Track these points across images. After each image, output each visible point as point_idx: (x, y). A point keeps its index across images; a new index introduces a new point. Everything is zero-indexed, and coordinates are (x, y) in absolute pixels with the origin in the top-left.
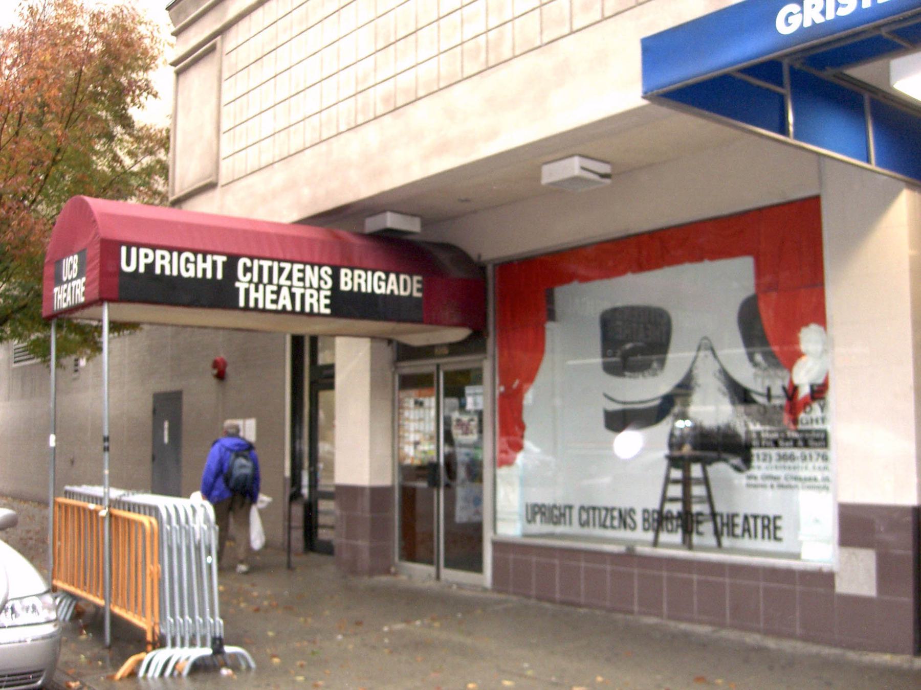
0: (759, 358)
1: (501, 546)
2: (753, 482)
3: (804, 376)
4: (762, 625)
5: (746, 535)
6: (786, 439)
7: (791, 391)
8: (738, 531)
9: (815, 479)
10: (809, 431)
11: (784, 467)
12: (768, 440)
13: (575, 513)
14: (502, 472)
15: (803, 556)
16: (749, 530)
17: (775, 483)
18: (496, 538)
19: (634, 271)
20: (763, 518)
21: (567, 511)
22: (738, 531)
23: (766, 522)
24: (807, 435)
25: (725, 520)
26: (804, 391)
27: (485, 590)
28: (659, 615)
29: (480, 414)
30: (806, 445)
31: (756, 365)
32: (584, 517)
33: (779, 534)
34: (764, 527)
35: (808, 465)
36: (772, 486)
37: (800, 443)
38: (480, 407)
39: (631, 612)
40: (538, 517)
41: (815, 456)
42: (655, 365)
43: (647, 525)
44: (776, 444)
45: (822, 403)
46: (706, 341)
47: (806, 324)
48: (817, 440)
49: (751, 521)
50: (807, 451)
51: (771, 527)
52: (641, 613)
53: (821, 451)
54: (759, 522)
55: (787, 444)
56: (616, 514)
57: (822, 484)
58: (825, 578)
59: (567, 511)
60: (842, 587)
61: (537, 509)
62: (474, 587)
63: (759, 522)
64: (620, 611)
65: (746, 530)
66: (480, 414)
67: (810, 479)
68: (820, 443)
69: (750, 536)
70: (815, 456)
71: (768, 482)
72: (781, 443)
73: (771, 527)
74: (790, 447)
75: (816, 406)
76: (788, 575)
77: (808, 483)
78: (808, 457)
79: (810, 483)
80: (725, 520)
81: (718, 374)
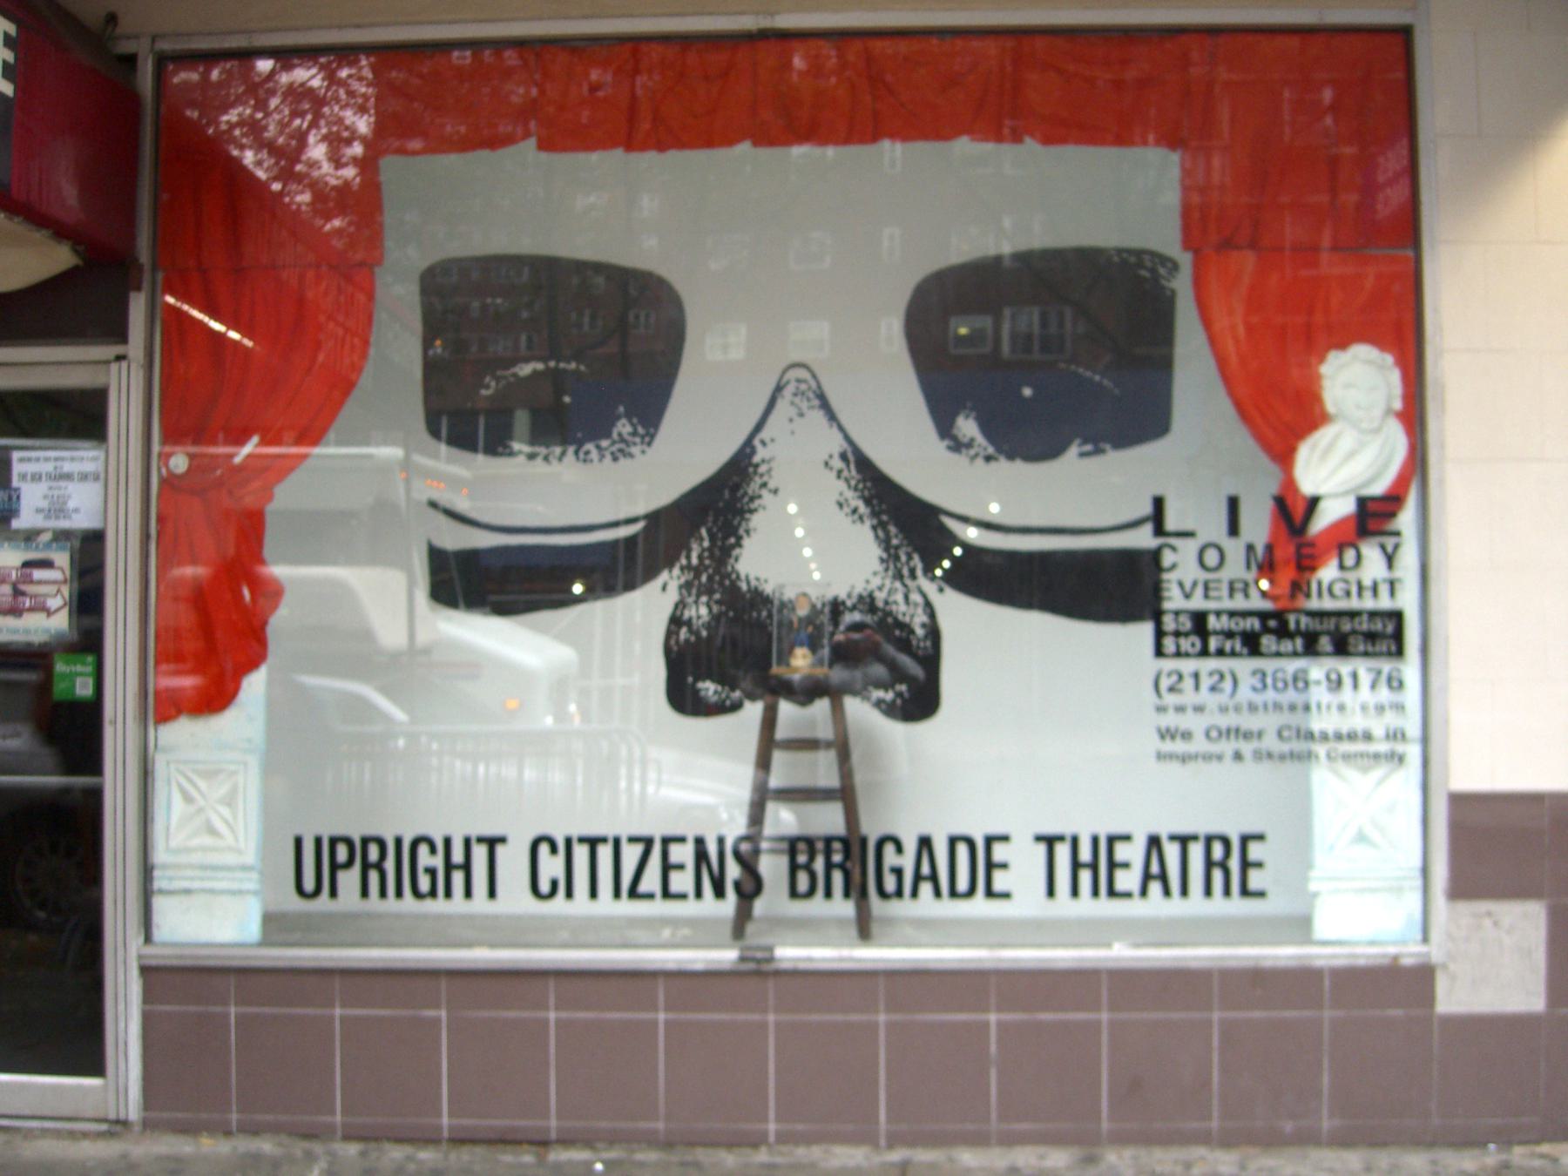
0: (967, 427)
1: (178, 981)
2: (1179, 746)
3: (1338, 467)
4: (1215, 1124)
5: (1155, 888)
6: (1283, 632)
7: (1293, 512)
8: (1127, 880)
9: (1368, 737)
10: (1353, 615)
11: (1277, 707)
12: (1229, 635)
13: (513, 861)
14: (182, 734)
15: (1321, 929)
16: (1163, 877)
17: (1247, 748)
18: (158, 954)
19: (765, 137)
20: (1209, 840)
21: (480, 853)
22: (1127, 880)
23: (1218, 851)
24: (1346, 626)
25: (1085, 855)
26: (1335, 510)
27: (119, 1127)
28: (864, 1137)
29: (89, 551)
30: (1341, 648)
31: (958, 446)
32: (551, 866)
33: (1255, 880)
34: (1209, 864)
35: (1344, 695)
36: (1238, 756)
37: (1325, 643)
38: (83, 519)
39: (756, 1141)
40: (349, 880)
41: (1365, 679)
42: (623, 427)
43: (803, 882)
44: (1252, 644)
45: (1390, 542)
46: (802, 373)
47: (1343, 345)
48: (1371, 637)
49: (1172, 852)
50: (1345, 667)
51: (1234, 864)
52: (784, 1138)
53: (1386, 666)
54: (1196, 852)
55: (1287, 646)
56: (683, 854)
57: (1383, 747)
58: (1406, 983)
59: (480, 853)
60: (1451, 999)
61: (342, 853)
62: (67, 1125)
63: (1196, 852)
64: (732, 1143)
65: (1154, 875)
66: (89, 551)
67: (1352, 737)
68: (1382, 646)
69: (1167, 892)
70: (1365, 679)
71: (1227, 747)
72: (1268, 642)
73: (1234, 864)
74: (1295, 654)
75: (1371, 552)
76: (1301, 983)
77: (1346, 747)
78: (1347, 681)
79: (1354, 747)
80: (1085, 855)
81: (838, 463)
